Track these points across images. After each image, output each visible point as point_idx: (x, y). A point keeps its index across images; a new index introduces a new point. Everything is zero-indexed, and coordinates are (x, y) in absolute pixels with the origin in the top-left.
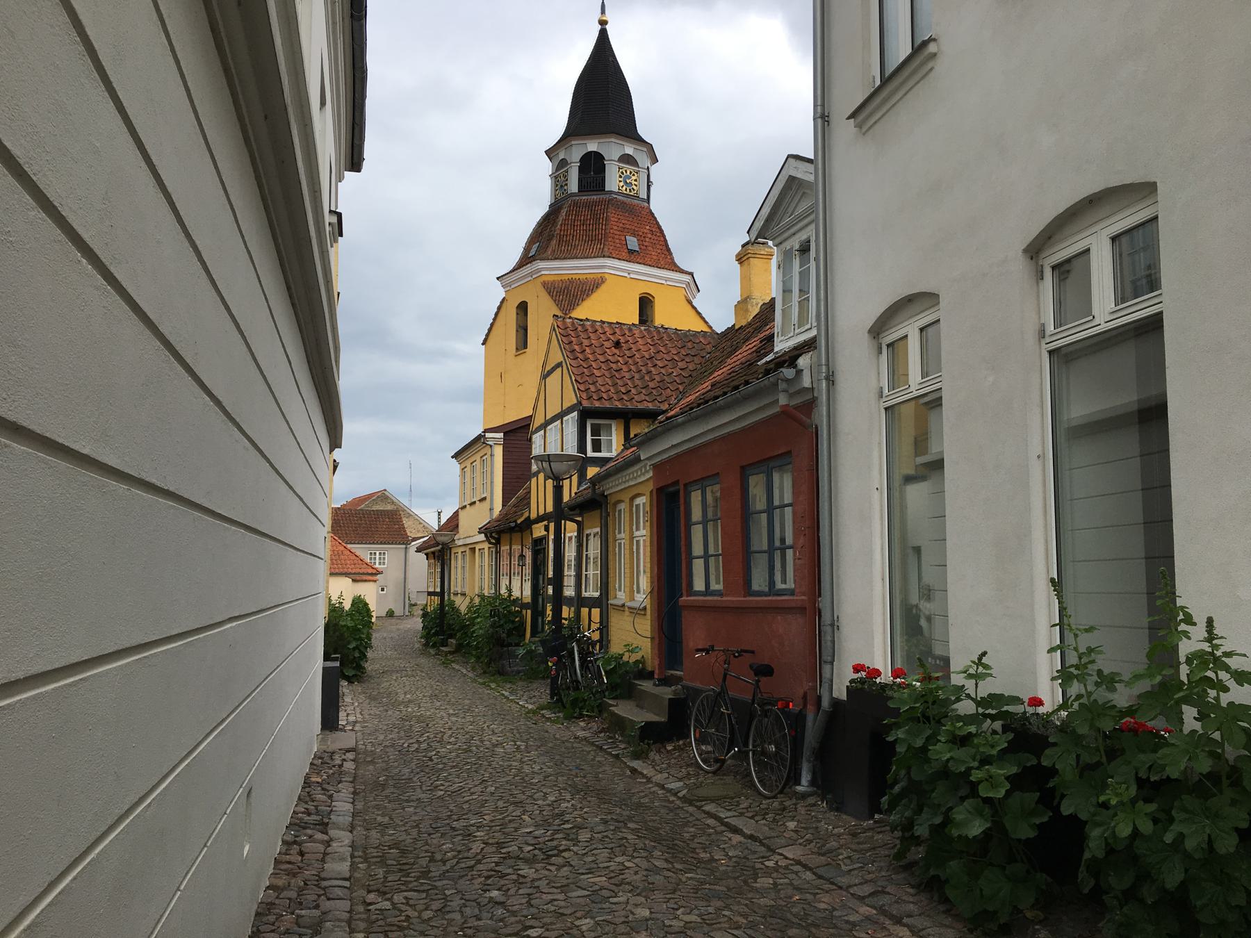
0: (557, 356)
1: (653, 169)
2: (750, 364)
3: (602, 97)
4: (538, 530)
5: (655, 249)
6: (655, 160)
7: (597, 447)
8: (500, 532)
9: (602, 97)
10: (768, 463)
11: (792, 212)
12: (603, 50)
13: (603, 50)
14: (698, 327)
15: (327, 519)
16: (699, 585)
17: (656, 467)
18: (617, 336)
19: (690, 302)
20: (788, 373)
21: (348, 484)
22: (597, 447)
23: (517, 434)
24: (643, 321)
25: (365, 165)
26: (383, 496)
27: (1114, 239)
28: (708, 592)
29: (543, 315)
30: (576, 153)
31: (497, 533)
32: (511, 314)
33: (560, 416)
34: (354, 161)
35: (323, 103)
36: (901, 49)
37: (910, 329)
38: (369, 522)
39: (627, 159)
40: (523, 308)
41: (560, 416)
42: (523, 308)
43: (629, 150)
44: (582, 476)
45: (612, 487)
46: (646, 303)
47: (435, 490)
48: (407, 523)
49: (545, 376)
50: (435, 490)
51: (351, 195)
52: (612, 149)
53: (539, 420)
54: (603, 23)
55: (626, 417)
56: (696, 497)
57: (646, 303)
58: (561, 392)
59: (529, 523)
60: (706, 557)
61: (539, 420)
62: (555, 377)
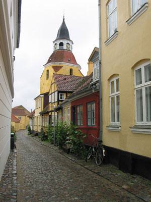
0: (54, 81)
1: (73, 45)
2: (89, 84)
3: (63, 33)
4: (50, 114)
5: (72, 59)
6: (73, 43)
7: (61, 98)
8: (43, 114)
9: (63, 33)
10: (91, 102)
11: (94, 57)
12: (64, 23)
13: (64, 23)
14: (81, 76)
15: (11, 110)
16: (79, 124)
17: (72, 102)
18: (65, 78)
19: (79, 70)
20: (94, 86)
21: (16, 103)
22: (61, 98)
23: (46, 96)
24: (70, 74)
25: (19, 47)
26: (21, 106)
27: (145, 67)
28: (80, 125)
29: (52, 71)
30: (58, 42)
31: (42, 114)
32: (46, 72)
33: (54, 92)
34: (18, 47)
35: (11, 15)
36: (112, 32)
37: (114, 80)
38: (19, 111)
39: (68, 43)
40: (48, 71)
41: (54, 92)
42: (48, 71)
43: (68, 42)
44: (58, 104)
45: (63, 106)
46: (71, 70)
47: (31, 105)
48: (26, 112)
49: (51, 85)
50: (31, 105)
51: (17, 53)
52: (65, 42)
53: (50, 93)
54: (64, 19)
55: (66, 92)
56: (78, 108)
57: (71, 70)
58: (54, 88)
59: (48, 112)
60: (80, 119)
61: (50, 93)
62: (53, 85)
